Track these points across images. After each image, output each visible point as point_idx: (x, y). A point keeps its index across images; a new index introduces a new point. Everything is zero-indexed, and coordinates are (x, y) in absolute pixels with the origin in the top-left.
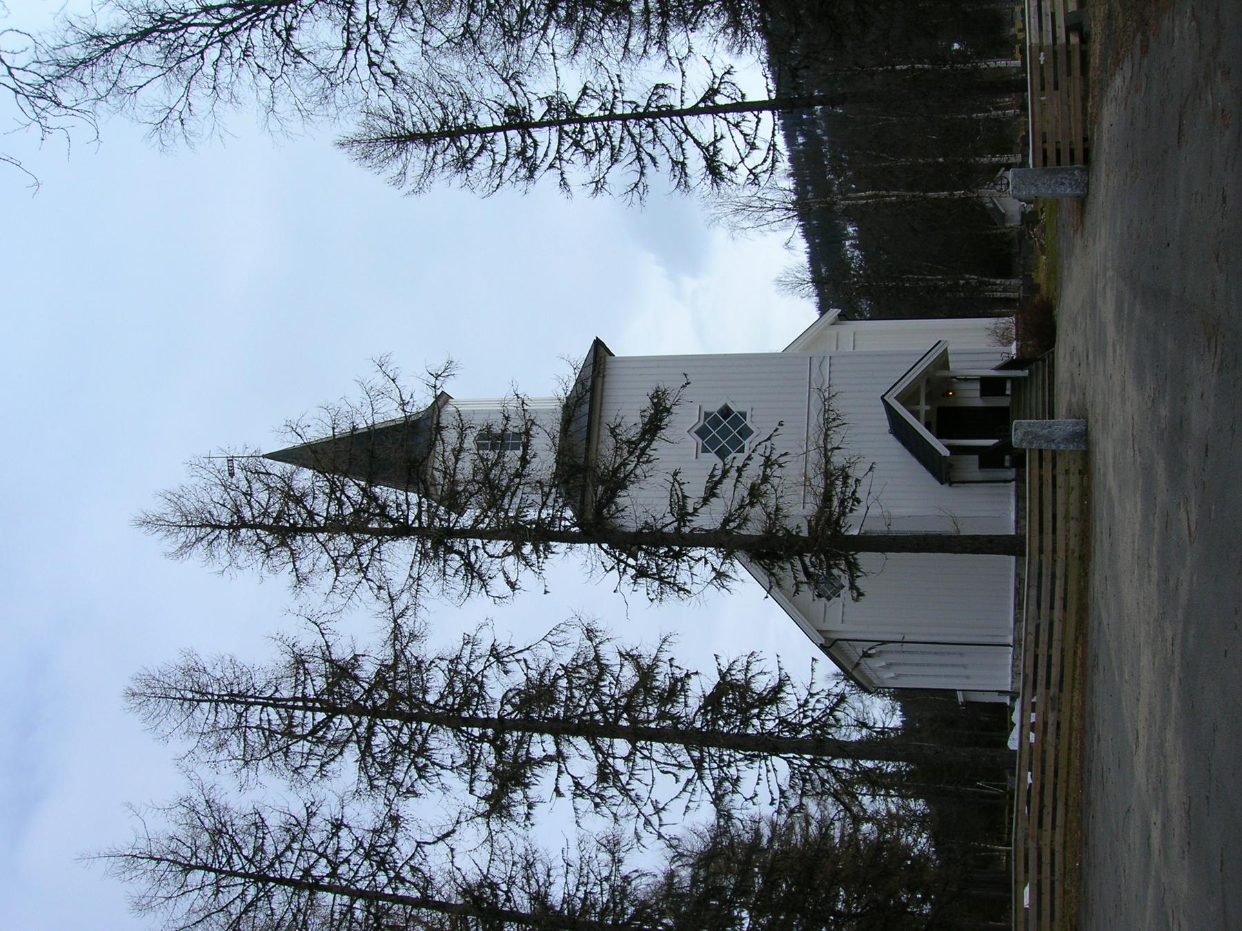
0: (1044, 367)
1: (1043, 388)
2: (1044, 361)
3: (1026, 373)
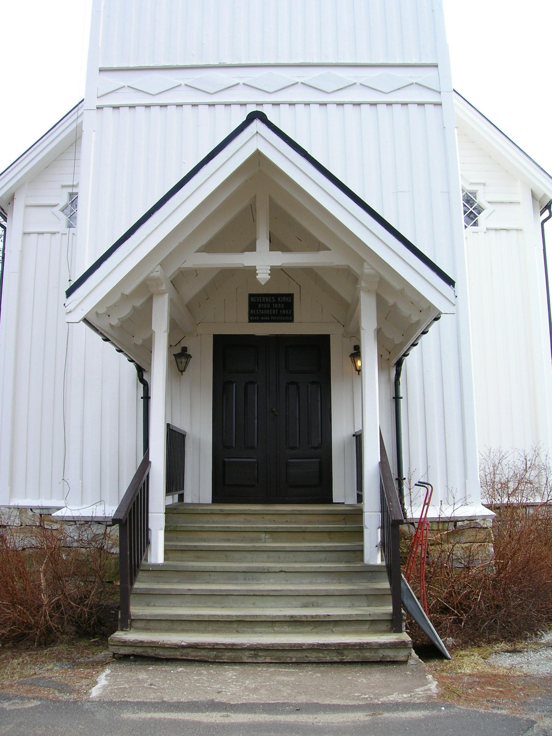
0: (373, 624)
1: (295, 623)
2: (394, 624)
3: (374, 557)
